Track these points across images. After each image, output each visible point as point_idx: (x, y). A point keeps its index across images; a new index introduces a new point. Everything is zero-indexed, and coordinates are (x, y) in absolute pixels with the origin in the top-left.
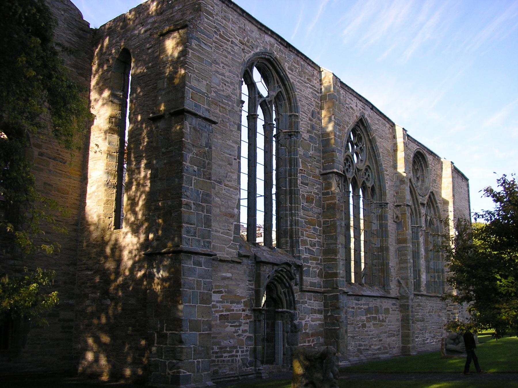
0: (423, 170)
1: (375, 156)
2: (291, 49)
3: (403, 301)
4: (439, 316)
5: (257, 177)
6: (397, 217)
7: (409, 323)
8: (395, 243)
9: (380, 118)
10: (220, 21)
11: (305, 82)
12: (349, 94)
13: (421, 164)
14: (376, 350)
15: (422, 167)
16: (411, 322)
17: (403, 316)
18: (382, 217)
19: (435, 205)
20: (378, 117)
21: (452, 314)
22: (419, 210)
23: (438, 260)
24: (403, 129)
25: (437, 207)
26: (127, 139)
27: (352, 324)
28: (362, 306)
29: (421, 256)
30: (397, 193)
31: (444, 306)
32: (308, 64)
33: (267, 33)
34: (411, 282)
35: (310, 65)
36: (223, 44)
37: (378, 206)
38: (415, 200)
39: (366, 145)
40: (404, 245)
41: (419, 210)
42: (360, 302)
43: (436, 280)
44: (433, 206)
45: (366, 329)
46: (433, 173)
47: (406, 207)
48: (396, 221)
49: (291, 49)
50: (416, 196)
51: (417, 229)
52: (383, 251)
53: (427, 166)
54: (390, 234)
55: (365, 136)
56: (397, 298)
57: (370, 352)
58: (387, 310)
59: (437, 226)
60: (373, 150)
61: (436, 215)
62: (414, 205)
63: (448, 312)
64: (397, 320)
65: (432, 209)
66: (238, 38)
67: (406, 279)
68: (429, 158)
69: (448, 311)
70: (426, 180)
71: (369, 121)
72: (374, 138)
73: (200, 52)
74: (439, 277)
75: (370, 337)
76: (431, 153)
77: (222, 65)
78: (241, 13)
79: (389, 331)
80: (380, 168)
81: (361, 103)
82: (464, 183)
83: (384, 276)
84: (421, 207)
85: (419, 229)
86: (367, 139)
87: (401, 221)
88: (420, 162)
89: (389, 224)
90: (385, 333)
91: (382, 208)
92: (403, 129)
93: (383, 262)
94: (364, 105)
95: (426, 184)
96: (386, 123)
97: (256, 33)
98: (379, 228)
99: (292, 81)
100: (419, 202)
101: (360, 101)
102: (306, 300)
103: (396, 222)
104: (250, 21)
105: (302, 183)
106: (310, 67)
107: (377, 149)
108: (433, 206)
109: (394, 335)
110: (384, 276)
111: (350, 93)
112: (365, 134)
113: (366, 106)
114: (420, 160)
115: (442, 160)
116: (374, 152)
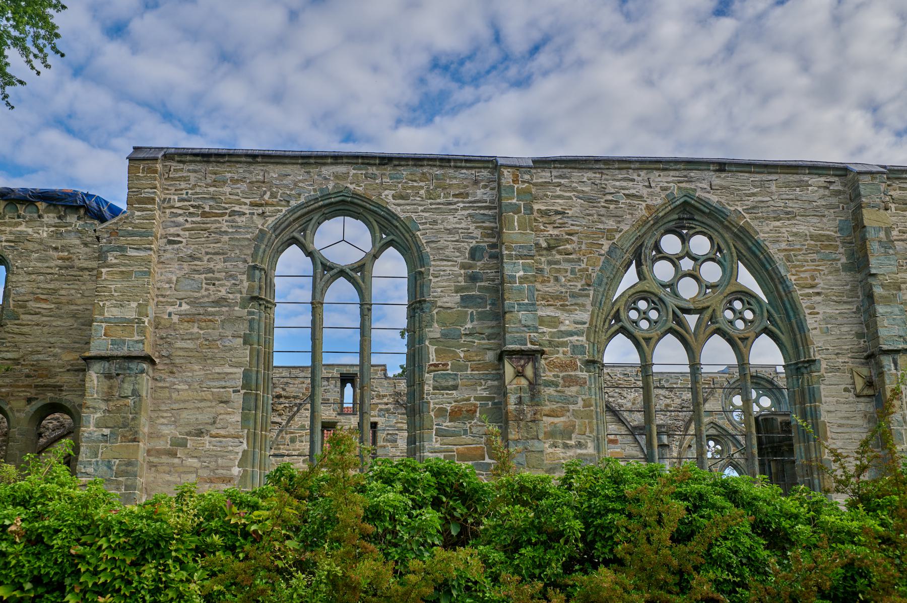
2: (397, 163)
9: (765, 177)
10: (201, 193)
11: (450, 204)
12: (617, 172)
24: (64, 7)
32: (456, 167)
33: (325, 164)
35: (462, 168)
36: (209, 225)
37: (794, 372)
39: (729, 249)
49: (397, 163)
66: (247, 201)
67: (781, 283)
73: (125, 265)
77: (206, 258)
78: (250, 160)
81: (672, 173)
89: (823, 408)
92: (64, 7)
94: (685, 173)
96: (806, 178)
97: (296, 173)
99: (402, 216)
104: (277, 163)
105: (435, 388)
106: (464, 171)
111: (619, 169)
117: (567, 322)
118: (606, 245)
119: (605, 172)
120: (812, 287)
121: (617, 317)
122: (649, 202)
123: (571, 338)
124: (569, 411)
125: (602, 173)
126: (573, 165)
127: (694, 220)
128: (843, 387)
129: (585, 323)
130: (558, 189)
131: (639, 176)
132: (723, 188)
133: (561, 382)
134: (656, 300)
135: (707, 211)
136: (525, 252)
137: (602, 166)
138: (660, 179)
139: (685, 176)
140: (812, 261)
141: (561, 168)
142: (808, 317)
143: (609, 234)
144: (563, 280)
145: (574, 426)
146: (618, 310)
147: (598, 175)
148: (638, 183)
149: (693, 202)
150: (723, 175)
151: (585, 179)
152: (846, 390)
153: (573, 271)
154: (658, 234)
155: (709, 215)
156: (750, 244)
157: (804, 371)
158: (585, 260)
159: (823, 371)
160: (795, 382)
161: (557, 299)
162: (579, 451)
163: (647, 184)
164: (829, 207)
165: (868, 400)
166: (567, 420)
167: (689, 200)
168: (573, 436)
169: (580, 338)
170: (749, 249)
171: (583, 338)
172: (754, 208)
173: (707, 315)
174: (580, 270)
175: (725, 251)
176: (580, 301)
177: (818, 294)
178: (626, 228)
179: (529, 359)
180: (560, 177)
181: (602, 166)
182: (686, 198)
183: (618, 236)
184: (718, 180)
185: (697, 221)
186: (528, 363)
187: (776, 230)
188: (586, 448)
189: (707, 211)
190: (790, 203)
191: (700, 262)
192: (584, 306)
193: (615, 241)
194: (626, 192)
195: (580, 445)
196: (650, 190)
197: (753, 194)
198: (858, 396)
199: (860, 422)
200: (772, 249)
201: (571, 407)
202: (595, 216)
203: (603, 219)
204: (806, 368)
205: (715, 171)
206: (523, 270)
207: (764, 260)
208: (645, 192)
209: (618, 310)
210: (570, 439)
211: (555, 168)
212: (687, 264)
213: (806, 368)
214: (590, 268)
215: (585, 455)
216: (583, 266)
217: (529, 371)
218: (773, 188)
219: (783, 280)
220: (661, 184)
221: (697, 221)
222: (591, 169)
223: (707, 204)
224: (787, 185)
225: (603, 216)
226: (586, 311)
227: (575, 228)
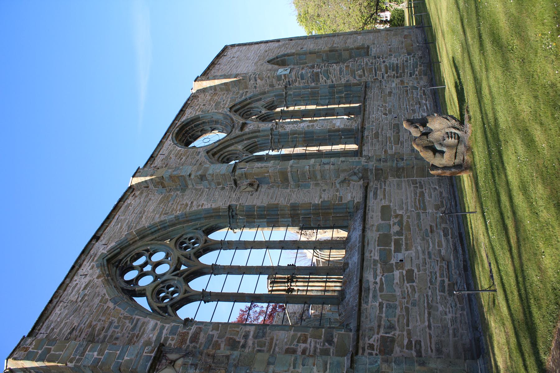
0: (204, 123)
1: (165, 227)
3: (371, 177)
4: (390, 93)
5: (245, 276)
6: (251, 185)
7: (403, 168)
8: (287, 188)
12: (66, 292)
13: (195, 126)
14: (448, 241)
15: (199, 124)
16: (401, 164)
17: (393, 176)
18: (248, 215)
19: (249, 101)
20: (113, 223)
21: (387, 73)
22: (249, 134)
23: (318, 93)
25: (250, 98)
26: (313, 107)
27: (407, 309)
28: (378, 280)
29: (311, 128)
30: (219, 184)
31: (378, 84)
34: (342, 162)
37: (234, 220)
38: (236, 140)
39: (148, 245)
40: (289, 175)
41: (249, 134)
42: (372, 287)
43: (343, 95)
44: (249, 104)
45: (416, 270)
46: (207, 107)
47: (236, 173)
48: (256, 187)
50: (231, 139)
51: (276, 135)
52: (298, 214)
53: (197, 119)
54: (273, 201)
55: (134, 247)
56: (366, 188)
57: (452, 257)
58: (385, 211)
59: (275, 96)
60: (155, 231)
61: (260, 99)
62: (243, 141)
63: (385, 78)
64: (399, 185)
65: (253, 105)
68: (189, 114)
69: (383, 78)
70: (215, 118)
71: (113, 244)
72: (139, 232)
74: (341, 92)
75: (427, 260)
76: (182, 111)
79: (416, 208)
80: (181, 220)
81: (85, 263)
82: (229, 53)
83: (334, 213)
84: (246, 130)
85: (275, 132)
86: (139, 244)
87: (256, 179)
88: (192, 127)
89: (259, 204)
90: (418, 215)
91: (236, 214)
93: (313, 214)
94: (89, 256)
95: (220, 117)
96: (126, 204)
98: (265, 220)
100: (240, 133)
101: (80, 266)
102: (378, 304)
103: (258, 187)
107: (155, 225)
108: (249, 104)
109: (422, 194)
110: (334, 213)
111: (65, 291)
112: (132, 248)
113: (92, 252)
114: (189, 129)
115: (194, 91)
116: (159, 229)
117: (151, 336)
118: (111, 305)
119: (61, 299)
120: (187, 205)
121: (164, 309)
122: (95, 277)
123: (164, 334)
124: (217, 341)
125: (61, 301)
126: (45, 318)
127: (121, 260)
128: (249, 196)
129: (157, 324)
130: (55, 330)
131: (76, 280)
132: (109, 240)
133: (193, 344)
134: (161, 285)
135: (119, 250)
136: (82, 349)
137: (57, 300)
138: (86, 268)
139: (91, 256)
140: (172, 204)
141: (42, 326)
142: (203, 207)
143: (103, 301)
144: (119, 334)
145: (231, 338)
146: (158, 307)
147: (61, 304)
148: (80, 281)
149: (109, 256)
150: (102, 238)
151: (59, 312)
152: (252, 195)
153: (116, 327)
154: (121, 280)
155: (122, 249)
156: (150, 232)
157: (234, 213)
158: (113, 318)
159: (237, 203)
160: (241, 221)
161: (131, 340)
162: (251, 337)
163: (83, 277)
164: (147, 196)
165: (260, 187)
166: (224, 343)
167: (107, 258)
168: (238, 340)
169: (166, 328)
170: (152, 233)
171: (167, 326)
172: (129, 227)
173: (183, 259)
174: (118, 323)
175: (149, 248)
176: (139, 324)
177: (192, 203)
178: (105, 291)
179: (164, 356)
180: (48, 328)
181: (57, 300)
182: (105, 259)
183: (107, 297)
184: (103, 240)
185: (123, 258)
186: (166, 356)
187: (147, 218)
188: (249, 332)
189: (119, 250)
190: (135, 212)
191: (149, 261)
192: (144, 323)
193: (109, 298)
194: (82, 289)
195: (246, 336)
196: (88, 275)
197: (121, 227)
198: (257, 190)
199: (272, 191)
200: (157, 220)
201: (215, 339)
202: (87, 309)
203: (91, 304)
204: (233, 211)
205: (97, 241)
206: (94, 352)
207: (162, 226)
208: (88, 279)
209: (158, 307)
210: (239, 342)
211: (39, 330)
212: (148, 268)
213: (233, 211)
214: (120, 316)
215: (254, 333)
216: (116, 320)
217: (172, 357)
218: (123, 218)
219: (177, 217)
220: (88, 269)
221: (123, 258)
222: (54, 307)
223: (113, 249)
224: (125, 212)
225: (89, 304)
226: (148, 322)
227: (87, 323)
